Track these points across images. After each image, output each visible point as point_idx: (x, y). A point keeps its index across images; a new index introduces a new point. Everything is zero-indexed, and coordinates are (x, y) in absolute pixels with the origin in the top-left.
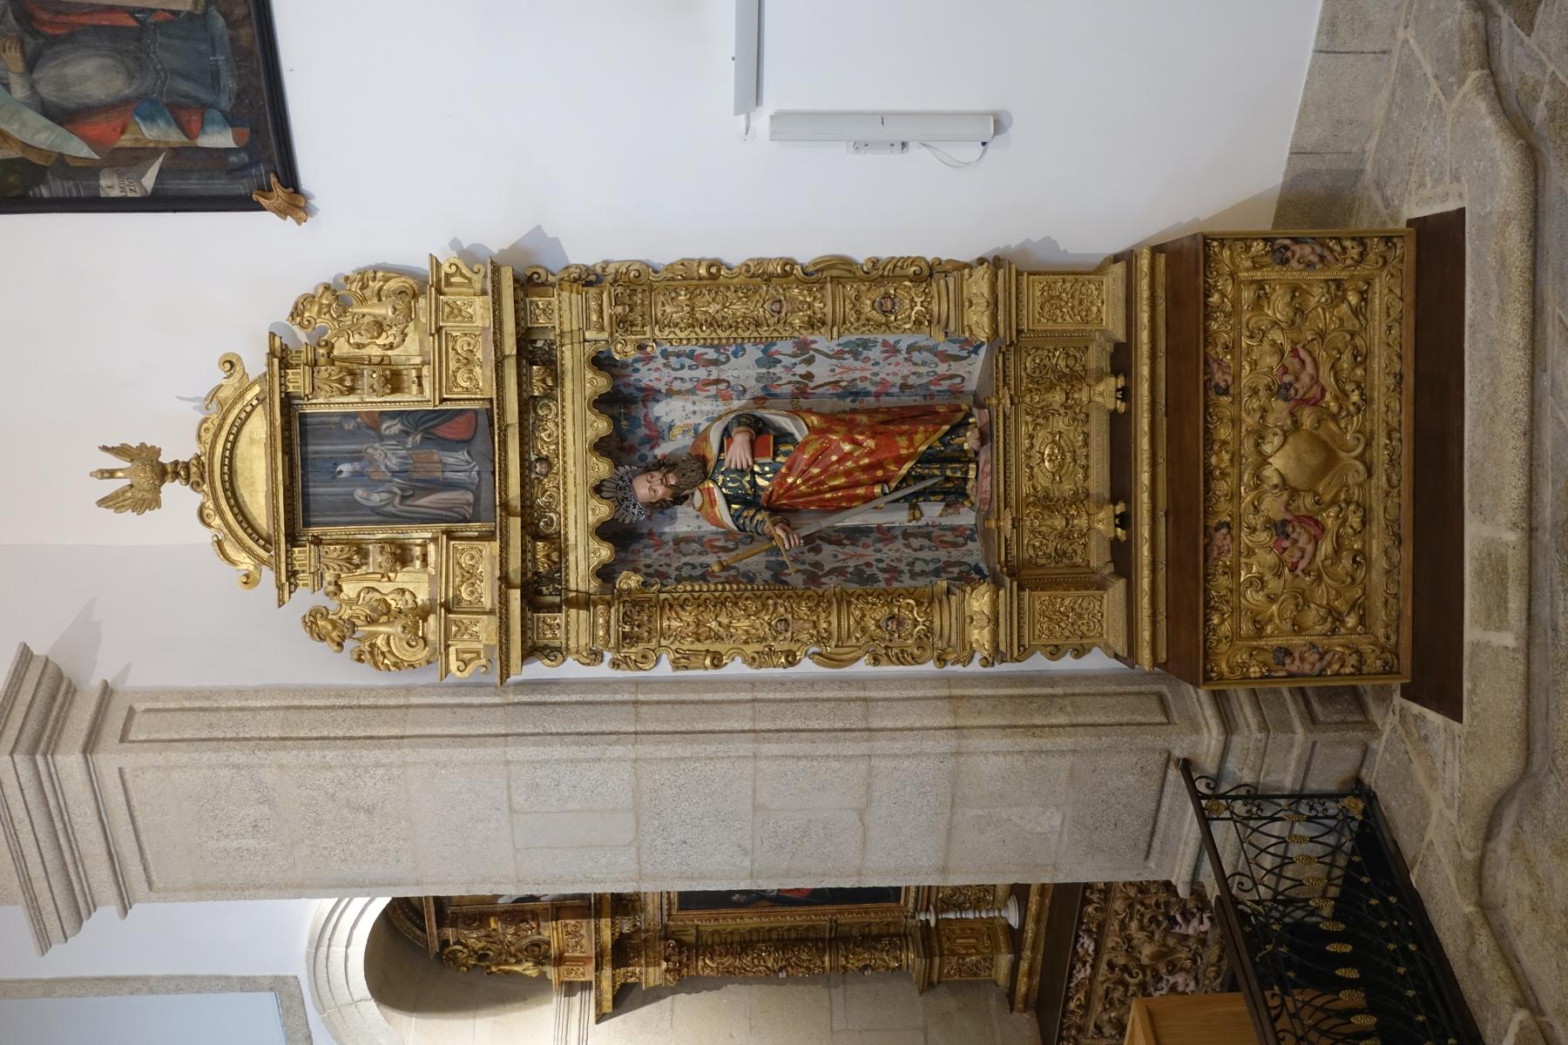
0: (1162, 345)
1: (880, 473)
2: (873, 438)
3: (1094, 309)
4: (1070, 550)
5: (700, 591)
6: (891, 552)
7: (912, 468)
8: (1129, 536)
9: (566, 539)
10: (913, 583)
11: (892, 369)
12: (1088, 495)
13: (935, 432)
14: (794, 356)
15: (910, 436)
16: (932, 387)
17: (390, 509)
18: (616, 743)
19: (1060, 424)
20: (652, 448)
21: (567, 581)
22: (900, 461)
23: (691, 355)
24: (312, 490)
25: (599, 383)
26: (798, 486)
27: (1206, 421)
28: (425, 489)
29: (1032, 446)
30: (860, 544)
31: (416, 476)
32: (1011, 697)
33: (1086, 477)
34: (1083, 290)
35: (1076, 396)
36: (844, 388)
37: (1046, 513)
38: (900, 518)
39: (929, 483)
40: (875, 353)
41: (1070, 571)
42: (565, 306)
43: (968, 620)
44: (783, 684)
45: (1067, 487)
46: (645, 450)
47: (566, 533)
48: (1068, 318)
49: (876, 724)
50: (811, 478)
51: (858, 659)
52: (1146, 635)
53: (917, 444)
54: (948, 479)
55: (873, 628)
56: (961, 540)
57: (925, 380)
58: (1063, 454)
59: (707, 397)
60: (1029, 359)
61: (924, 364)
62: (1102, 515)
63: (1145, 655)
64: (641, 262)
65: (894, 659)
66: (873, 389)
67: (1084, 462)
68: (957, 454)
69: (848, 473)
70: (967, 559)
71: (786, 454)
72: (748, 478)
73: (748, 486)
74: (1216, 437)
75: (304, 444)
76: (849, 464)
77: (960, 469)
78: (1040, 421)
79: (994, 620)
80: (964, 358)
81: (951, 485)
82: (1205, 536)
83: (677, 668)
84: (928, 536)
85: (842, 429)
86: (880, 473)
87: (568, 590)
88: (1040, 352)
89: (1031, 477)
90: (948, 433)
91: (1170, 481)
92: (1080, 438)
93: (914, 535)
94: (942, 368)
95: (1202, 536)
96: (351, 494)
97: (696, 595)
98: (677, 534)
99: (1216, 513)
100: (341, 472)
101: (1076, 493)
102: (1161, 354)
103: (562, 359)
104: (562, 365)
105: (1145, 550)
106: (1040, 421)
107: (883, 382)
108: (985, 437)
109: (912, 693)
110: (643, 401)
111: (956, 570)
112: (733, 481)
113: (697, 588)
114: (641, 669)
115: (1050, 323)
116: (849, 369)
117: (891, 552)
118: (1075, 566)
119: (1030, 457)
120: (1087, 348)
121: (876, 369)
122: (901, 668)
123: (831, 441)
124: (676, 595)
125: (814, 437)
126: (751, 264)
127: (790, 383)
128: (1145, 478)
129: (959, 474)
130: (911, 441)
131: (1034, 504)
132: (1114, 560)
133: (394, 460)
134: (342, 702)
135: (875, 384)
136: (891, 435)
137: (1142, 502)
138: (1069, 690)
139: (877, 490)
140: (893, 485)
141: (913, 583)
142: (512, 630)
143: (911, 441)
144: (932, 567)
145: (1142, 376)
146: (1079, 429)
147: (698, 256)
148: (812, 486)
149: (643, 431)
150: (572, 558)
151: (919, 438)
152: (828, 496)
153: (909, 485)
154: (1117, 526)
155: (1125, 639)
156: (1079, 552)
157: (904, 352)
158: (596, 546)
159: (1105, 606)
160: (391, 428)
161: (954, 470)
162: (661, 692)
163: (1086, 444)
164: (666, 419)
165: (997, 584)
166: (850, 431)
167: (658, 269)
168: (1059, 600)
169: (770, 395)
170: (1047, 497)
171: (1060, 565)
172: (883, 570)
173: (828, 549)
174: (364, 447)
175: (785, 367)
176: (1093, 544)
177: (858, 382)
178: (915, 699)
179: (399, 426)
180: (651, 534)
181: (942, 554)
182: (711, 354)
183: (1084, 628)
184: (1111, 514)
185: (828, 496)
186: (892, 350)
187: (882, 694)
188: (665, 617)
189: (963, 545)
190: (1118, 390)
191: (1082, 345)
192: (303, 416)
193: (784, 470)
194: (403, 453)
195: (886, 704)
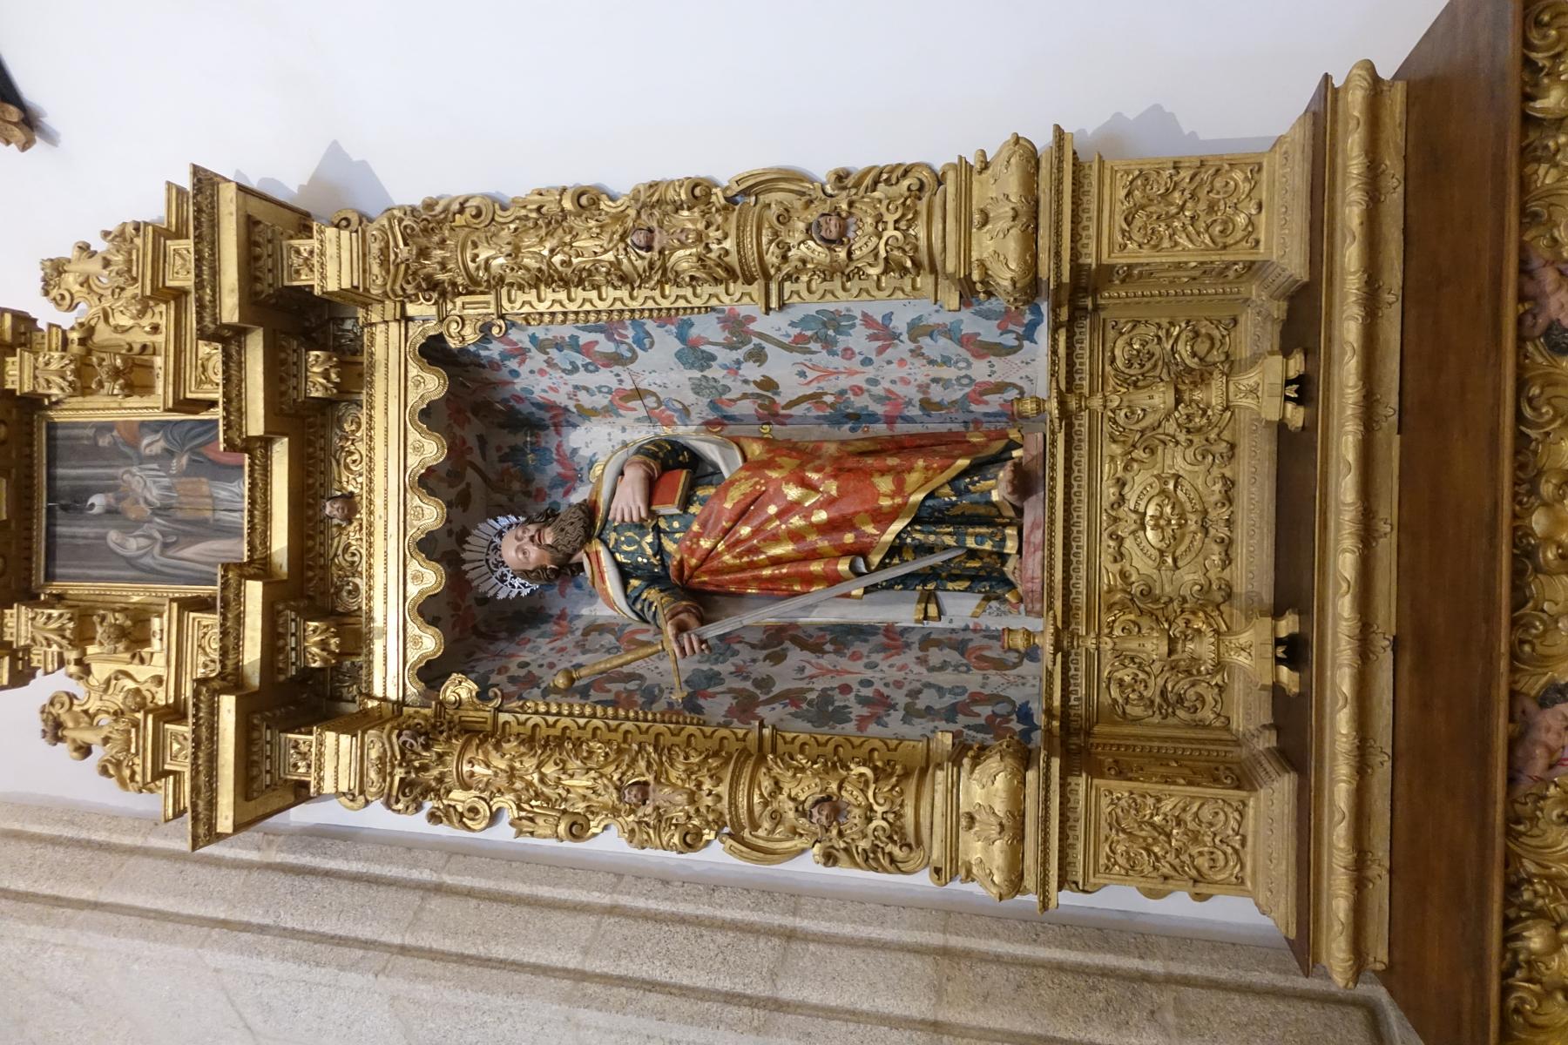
0: (1393, 278)
1: (849, 538)
2: (835, 477)
3: (1241, 220)
4: (1191, 694)
5: (559, 714)
6: (888, 671)
7: (904, 530)
8: (1305, 685)
9: (370, 619)
10: (905, 730)
11: (895, 371)
12: (1229, 595)
13: (943, 469)
14: (732, 347)
15: (899, 475)
16: (973, 407)
17: (147, 561)
18: (354, 966)
19: (1178, 461)
20: (567, 493)
21: (370, 683)
22: (883, 518)
23: (574, 344)
24: (60, 530)
25: (432, 385)
26: (720, 554)
27: (1519, 418)
28: (186, 534)
29: (1122, 499)
30: (848, 652)
31: (180, 515)
32: (1060, 967)
33: (1227, 561)
34: (1219, 183)
35: (1198, 395)
36: (832, 406)
37: (1145, 622)
38: (903, 612)
39: (937, 559)
40: (858, 339)
41: (1191, 734)
42: (331, 250)
43: (963, 822)
44: (666, 883)
45: (1189, 578)
46: (557, 495)
47: (370, 610)
48: (1183, 240)
49: (788, 993)
50: (739, 542)
51: (803, 851)
52: (1338, 905)
53: (908, 490)
54: (972, 554)
55: (791, 814)
56: (1013, 657)
57: (957, 394)
58: (1182, 516)
59: (638, 420)
60: (1120, 343)
61: (946, 361)
62: (1245, 638)
63: (1336, 951)
64: (484, 196)
65: (859, 860)
66: (880, 409)
67: (1223, 532)
68: (982, 511)
69: (795, 536)
70: (1011, 692)
71: (703, 501)
72: (649, 539)
73: (649, 551)
74: (1544, 461)
75: (51, 463)
76: (796, 521)
77: (991, 536)
78: (1139, 454)
79: (1015, 827)
80: (1013, 350)
81: (976, 564)
82: (1511, 719)
83: (520, 833)
84: (961, 647)
85: (789, 462)
86: (849, 538)
87: (370, 696)
88: (1141, 329)
89: (1119, 556)
90: (965, 473)
91: (1406, 572)
92: (1218, 487)
93: (938, 644)
94: (980, 370)
95: (1502, 720)
96: (104, 537)
97: (551, 719)
98: (597, 618)
99: (1544, 661)
100: (93, 505)
101: (1205, 590)
102: (1391, 297)
103: (372, 344)
104: (372, 354)
105: (1342, 723)
106: (1139, 454)
107: (889, 397)
108: (1025, 483)
109: (874, 932)
110: (556, 425)
111: (985, 711)
112: (630, 542)
113: (554, 709)
114: (469, 828)
115: (1146, 251)
116: (828, 373)
117: (888, 671)
118: (1201, 725)
119: (1116, 520)
120: (1235, 321)
121: (870, 372)
122: (872, 875)
123: (769, 480)
124: (523, 717)
125: (744, 474)
126: (642, 189)
127: (745, 396)
128: (1345, 563)
129: (988, 546)
130: (900, 489)
131: (1124, 608)
132: (1277, 727)
133: (155, 492)
134: (69, 832)
135: (879, 399)
136: (868, 473)
137: (1337, 617)
138: (1177, 969)
139: (843, 566)
140: (876, 559)
141: (905, 730)
142: (221, 761)
143: (900, 489)
144: (948, 700)
145: (1344, 342)
146: (1216, 472)
147: (560, 184)
148: (740, 556)
149: (554, 469)
150: (378, 646)
151: (913, 478)
152: (767, 572)
153: (903, 561)
154: (1279, 661)
155: (1292, 901)
156: (1209, 699)
157: (904, 337)
158: (417, 631)
159: (1250, 823)
160: (152, 444)
161: (980, 538)
162: (478, 873)
163: (1228, 499)
164: (585, 453)
165: (1025, 759)
166: (802, 467)
167: (507, 201)
168: (1150, 801)
169: (725, 417)
170: (1147, 593)
171: (1171, 720)
172: (864, 701)
173: (796, 656)
174: (121, 471)
175: (724, 367)
176: (1238, 688)
177: (850, 395)
178: (884, 946)
179: (162, 444)
180: (562, 616)
181: (973, 681)
182: (605, 346)
183: (1204, 863)
184: (1267, 636)
185: (767, 572)
186: (884, 334)
187: (822, 926)
188: (467, 756)
189: (1015, 666)
190: (1288, 382)
191: (1225, 315)
192: (52, 426)
193: (695, 528)
194: (166, 481)
195: (823, 950)
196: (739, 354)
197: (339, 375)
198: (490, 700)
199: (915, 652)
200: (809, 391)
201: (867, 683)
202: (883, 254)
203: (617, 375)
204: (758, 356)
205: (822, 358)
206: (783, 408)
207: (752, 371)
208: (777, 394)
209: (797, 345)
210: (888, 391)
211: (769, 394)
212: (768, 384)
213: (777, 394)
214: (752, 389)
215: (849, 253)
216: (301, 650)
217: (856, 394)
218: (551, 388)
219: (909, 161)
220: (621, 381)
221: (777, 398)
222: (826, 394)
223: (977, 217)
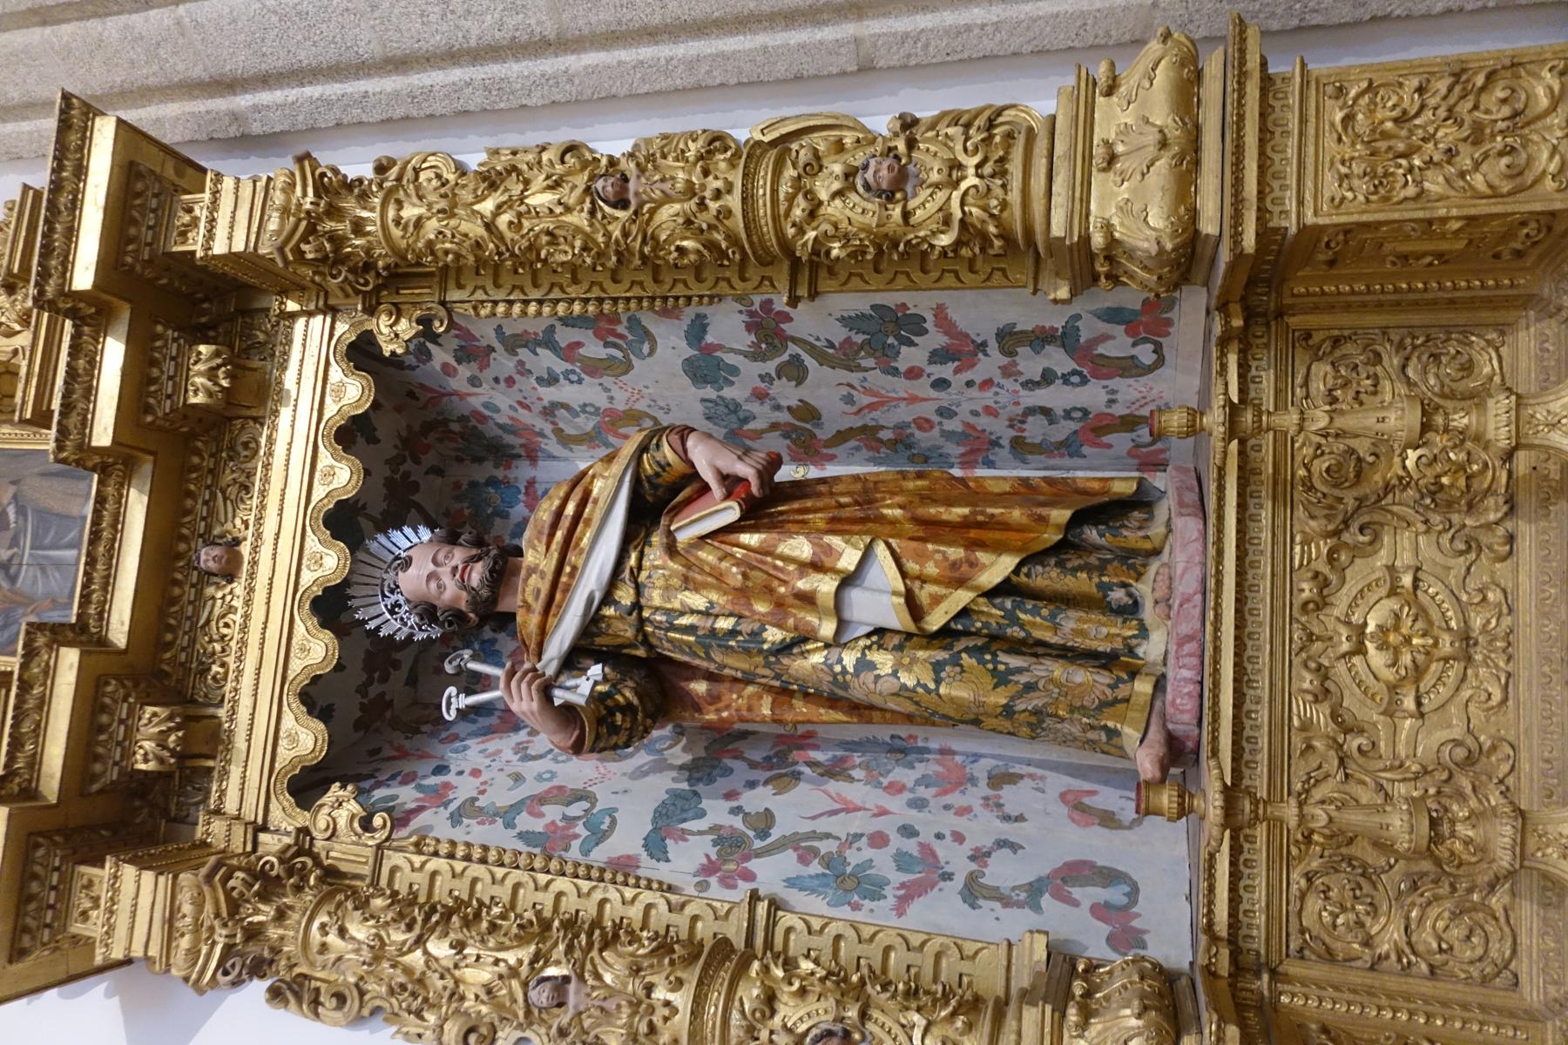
14: (755, 355)
25: (352, 392)
106: (1352, 536)
116: (882, 403)
121: (944, 398)
127: (774, 426)
177: (914, 430)
186: (960, 351)
196: (770, 367)
197: (228, 375)
198: (374, 830)
199: (983, 789)
200: (857, 422)
201: (908, 831)
202: (958, 214)
203: (607, 390)
204: (795, 371)
205: (877, 379)
206: (826, 446)
207: (787, 393)
208: (818, 426)
209: (842, 357)
210: (967, 425)
211: (808, 426)
212: (808, 412)
213: (818, 426)
214: (784, 417)
215: (906, 215)
216: (127, 747)
217: (920, 428)
218: (520, 403)
219: (1000, 103)
220: (611, 398)
221: (817, 432)
222: (883, 427)
223: (1099, 152)
